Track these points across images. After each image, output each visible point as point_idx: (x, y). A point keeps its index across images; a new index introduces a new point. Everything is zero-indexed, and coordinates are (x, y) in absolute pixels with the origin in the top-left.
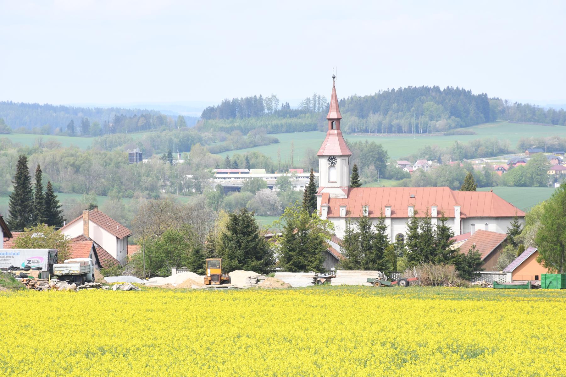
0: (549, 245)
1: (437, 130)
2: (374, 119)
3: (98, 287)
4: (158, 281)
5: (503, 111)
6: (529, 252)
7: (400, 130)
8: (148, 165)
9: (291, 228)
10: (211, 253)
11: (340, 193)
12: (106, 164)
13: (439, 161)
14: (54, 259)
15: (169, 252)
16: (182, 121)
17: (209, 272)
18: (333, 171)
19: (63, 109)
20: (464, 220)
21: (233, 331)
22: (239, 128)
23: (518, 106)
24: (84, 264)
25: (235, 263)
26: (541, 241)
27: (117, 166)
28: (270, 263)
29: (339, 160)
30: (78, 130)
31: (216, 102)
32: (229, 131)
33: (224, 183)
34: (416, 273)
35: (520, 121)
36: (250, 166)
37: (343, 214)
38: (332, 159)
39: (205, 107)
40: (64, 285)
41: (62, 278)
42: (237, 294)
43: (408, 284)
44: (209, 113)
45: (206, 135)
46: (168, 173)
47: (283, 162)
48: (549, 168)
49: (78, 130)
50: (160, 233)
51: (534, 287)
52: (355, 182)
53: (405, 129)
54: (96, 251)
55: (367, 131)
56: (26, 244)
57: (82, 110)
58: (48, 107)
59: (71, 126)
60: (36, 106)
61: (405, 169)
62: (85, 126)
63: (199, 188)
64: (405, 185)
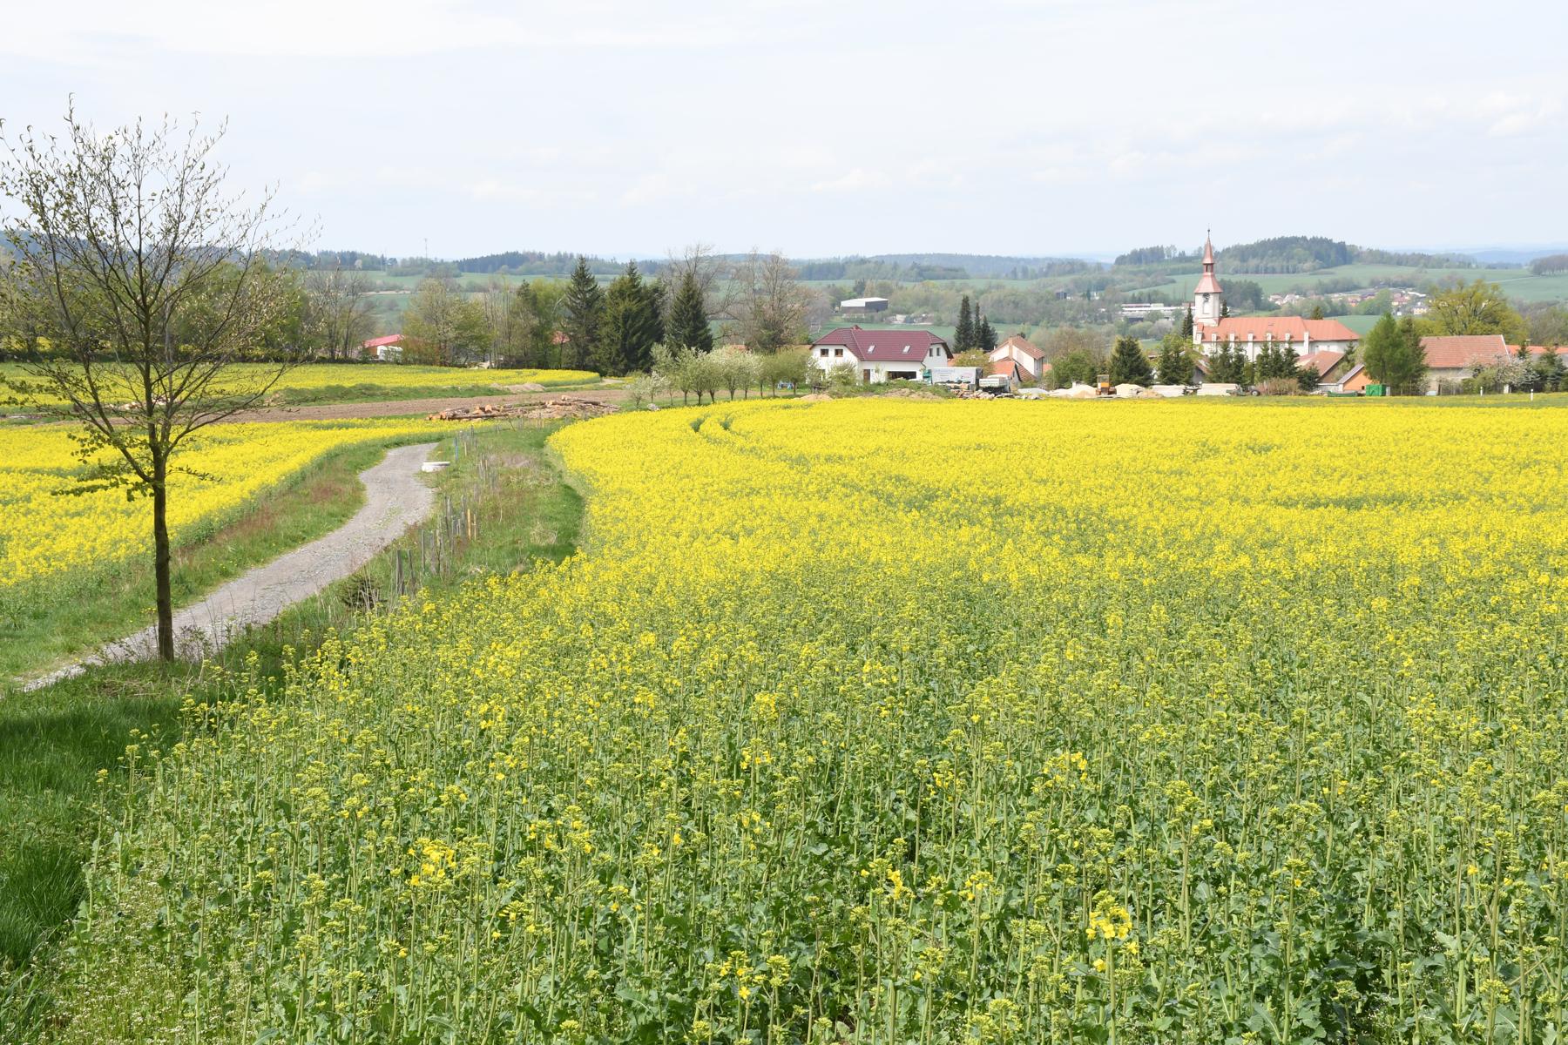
0: (1374, 362)
1: (1304, 271)
2: (1253, 262)
3: (1011, 397)
4: (1061, 392)
5: (1358, 255)
6: (1358, 367)
7: (1274, 271)
8: (1071, 302)
9: (1167, 350)
10: (1103, 370)
11: (1212, 323)
12: (1038, 301)
13: (1305, 295)
14: (980, 375)
15: (1073, 370)
16: (1099, 267)
17: (1100, 385)
18: (1206, 305)
19: (1010, 259)
20: (1313, 343)
21: (1085, 432)
22: (1145, 271)
23: (1371, 251)
24: (1002, 380)
25: (1122, 378)
26: (1368, 358)
27: (1047, 302)
28: (1151, 378)
29: (1211, 297)
30: (1020, 275)
31: (1127, 251)
32: (1135, 274)
33: (1130, 314)
34: (1265, 385)
35: (1371, 263)
36: (1151, 302)
37: (1214, 339)
38: (1206, 295)
39: (1118, 255)
40: (987, 395)
41: (986, 390)
42: (1122, 405)
43: (1259, 394)
44: (1121, 260)
45: (1118, 277)
46: (1086, 307)
47: (1178, 297)
48: (1393, 300)
49: (1020, 275)
50: (1066, 354)
51: (1360, 395)
52: (1224, 314)
53: (1278, 269)
54: (1018, 369)
55: (1247, 272)
56: (961, 364)
57: (1023, 259)
58: (998, 258)
59: (1014, 273)
60: (989, 258)
61: (1278, 303)
62: (1025, 271)
63: (1110, 319)
64: (1276, 316)
